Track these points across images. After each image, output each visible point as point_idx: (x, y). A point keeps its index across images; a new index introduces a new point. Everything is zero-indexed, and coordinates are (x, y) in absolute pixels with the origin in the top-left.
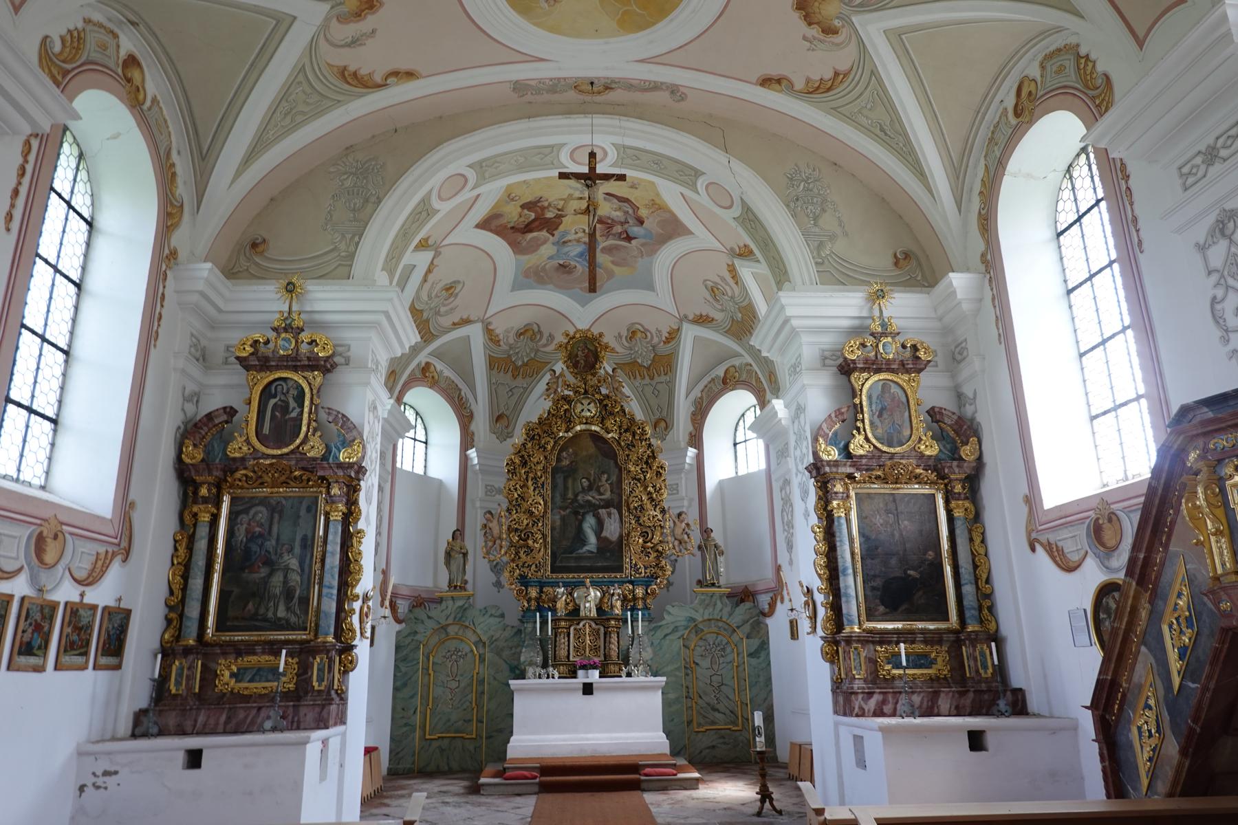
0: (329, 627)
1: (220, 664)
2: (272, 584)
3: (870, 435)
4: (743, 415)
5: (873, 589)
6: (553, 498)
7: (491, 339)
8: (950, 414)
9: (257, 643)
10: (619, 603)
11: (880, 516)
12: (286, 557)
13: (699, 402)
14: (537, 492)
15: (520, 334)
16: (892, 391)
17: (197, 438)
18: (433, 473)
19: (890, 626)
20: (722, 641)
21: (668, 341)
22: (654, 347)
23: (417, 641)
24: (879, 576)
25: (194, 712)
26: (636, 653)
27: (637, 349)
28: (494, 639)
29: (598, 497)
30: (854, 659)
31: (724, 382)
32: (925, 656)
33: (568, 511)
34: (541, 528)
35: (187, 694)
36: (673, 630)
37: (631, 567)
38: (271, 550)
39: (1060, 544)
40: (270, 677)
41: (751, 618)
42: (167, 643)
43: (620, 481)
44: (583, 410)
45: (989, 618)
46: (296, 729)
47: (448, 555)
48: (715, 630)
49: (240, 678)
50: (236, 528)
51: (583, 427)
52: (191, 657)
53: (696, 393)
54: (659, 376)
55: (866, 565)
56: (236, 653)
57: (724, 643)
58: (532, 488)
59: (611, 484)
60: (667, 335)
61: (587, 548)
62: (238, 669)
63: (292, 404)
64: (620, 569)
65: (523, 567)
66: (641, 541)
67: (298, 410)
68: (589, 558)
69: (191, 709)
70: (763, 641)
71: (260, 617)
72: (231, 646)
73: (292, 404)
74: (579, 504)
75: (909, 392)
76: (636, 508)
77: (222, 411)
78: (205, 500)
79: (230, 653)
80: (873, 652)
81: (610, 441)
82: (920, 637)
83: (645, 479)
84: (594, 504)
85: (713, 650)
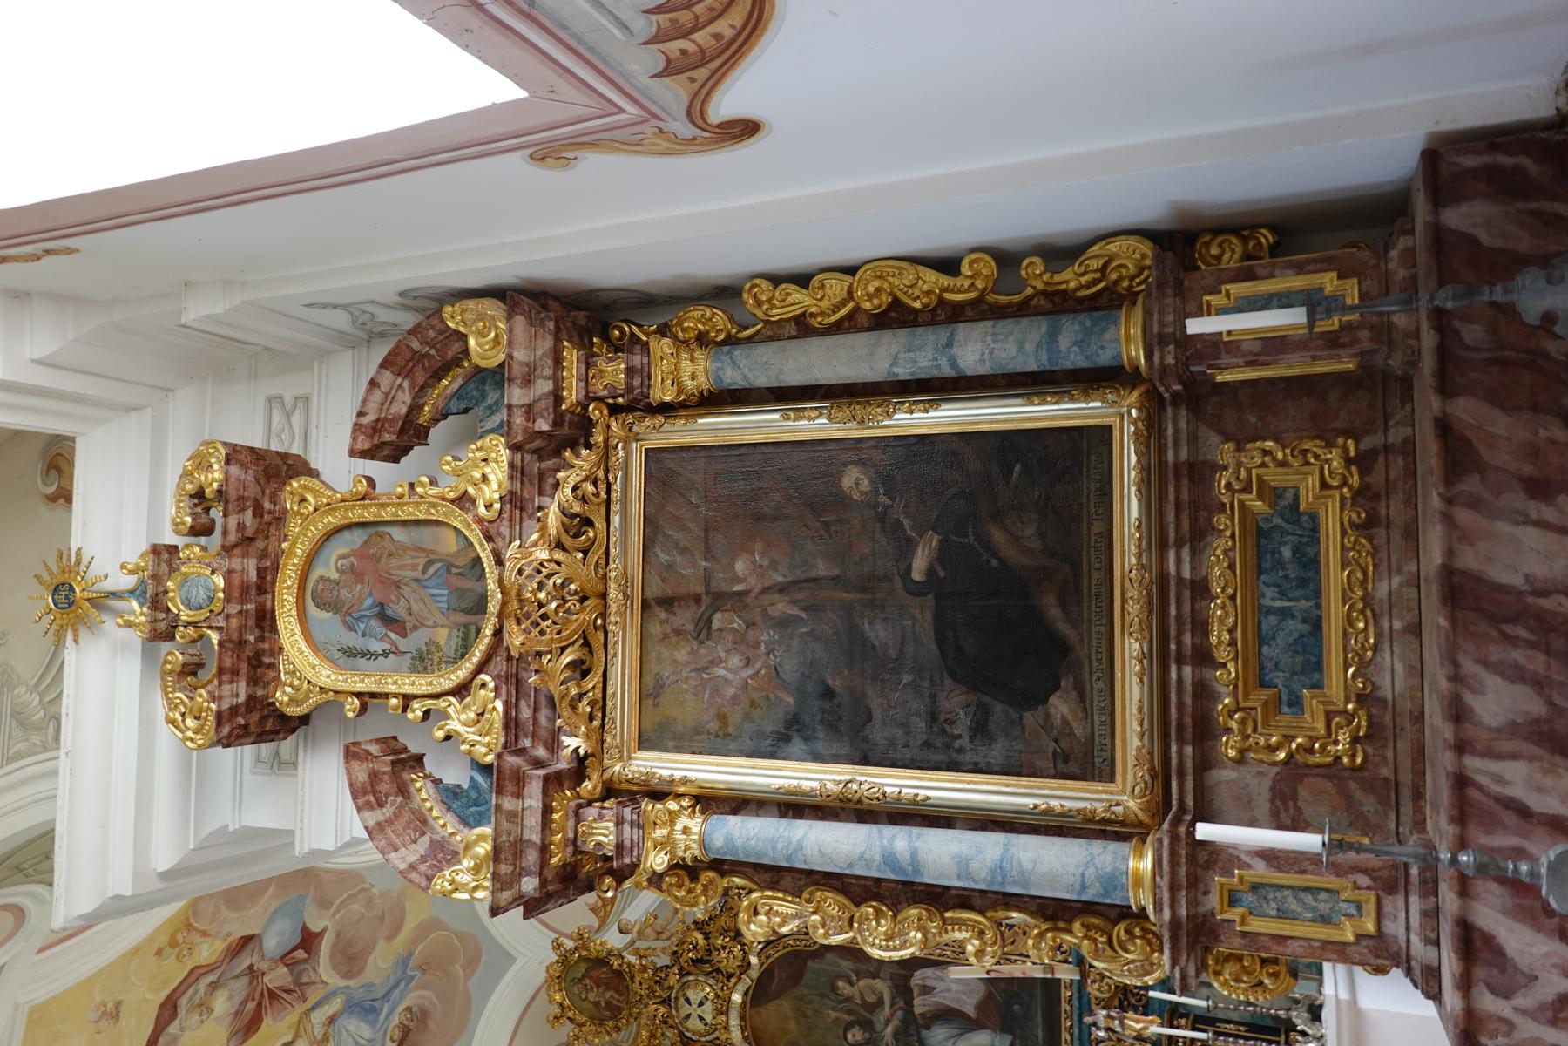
3: (447, 683)
5: (980, 729)
8: (378, 395)
11: (712, 663)
16: (335, 575)
19: (1132, 692)
24: (933, 698)
29: (887, 1011)
30: (1283, 915)
32: (1258, 537)
39: (644, 27)
45: (1095, 264)
46: (1318, 571)
51: (734, 1022)
55: (892, 743)
75: (332, 520)
80: (1246, 775)
82: (1179, 564)
84: (903, 1021)
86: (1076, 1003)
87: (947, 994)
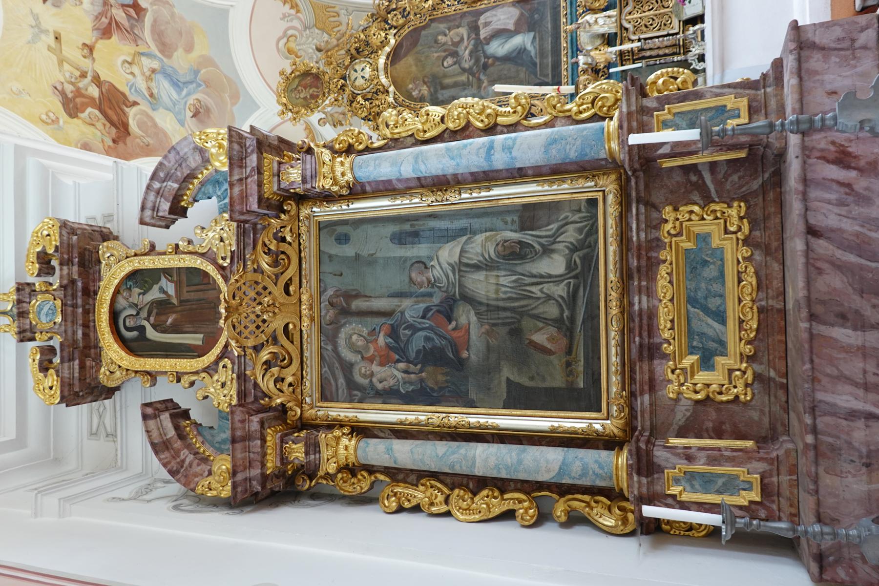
0: (589, 128)
1: (679, 393)
2: (493, 295)
9: (625, 309)
12: (437, 272)
17: (197, 469)
22: (306, 28)
25: (823, 422)
33: (482, 77)
35: (761, 459)
38: (423, 306)
40: (710, 272)
42: (625, 521)
43: (446, 19)
44: (363, 77)
49: (712, 345)
50: (380, 386)
52: (659, 454)
56: (651, 358)
59: (449, 29)
60: (288, 6)
61: (529, 47)
62: (692, 351)
63: (154, 294)
67: (164, 282)
68: (541, 39)
69: (814, 431)
71: (566, 313)
72: (632, 371)
73: (154, 294)
74: (474, 64)
77: (152, 423)
78: (313, 447)
79: (651, 372)
84: (474, 45)
86: (569, 16)
87: (498, 23)
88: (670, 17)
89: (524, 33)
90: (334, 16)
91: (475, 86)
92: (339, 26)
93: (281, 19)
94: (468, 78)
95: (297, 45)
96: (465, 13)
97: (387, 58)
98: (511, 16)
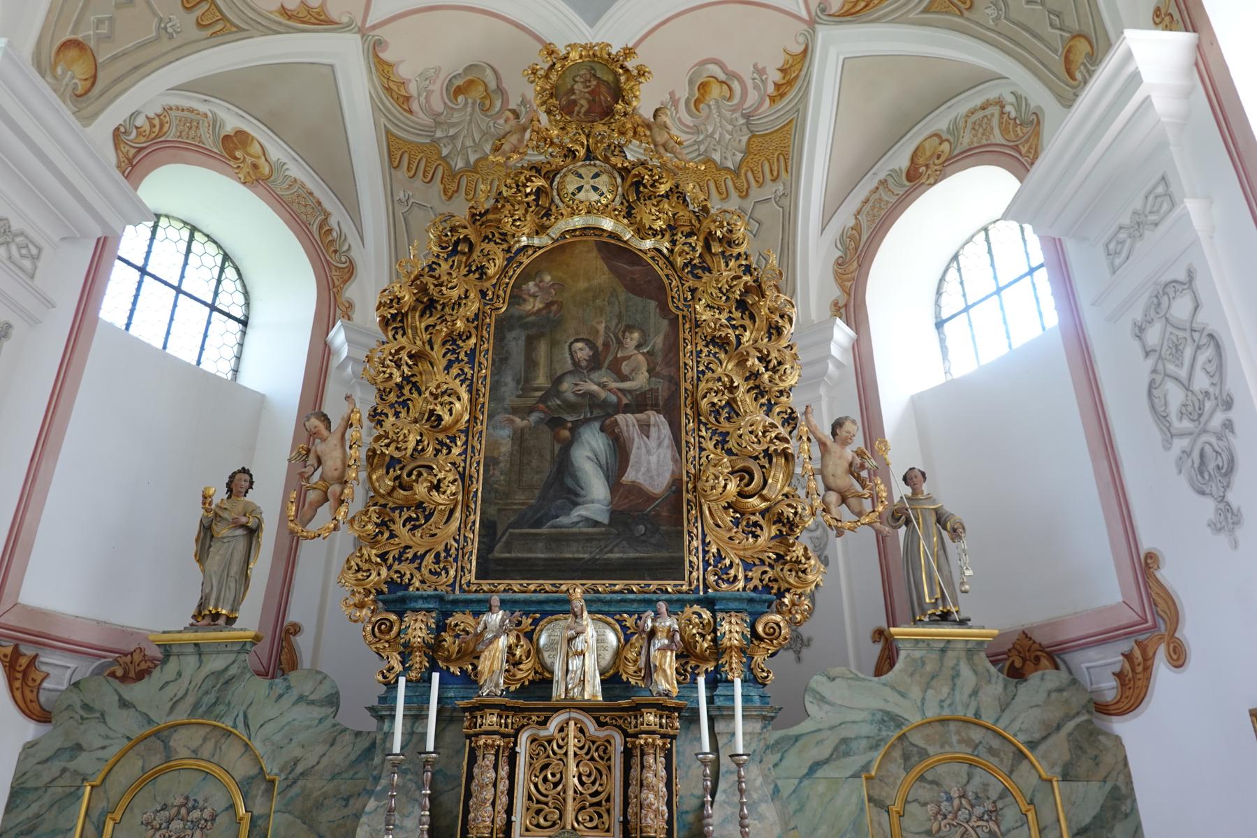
4: (955, 257)
6: (495, 387)
7: (389, 89)
10: (669, 662)
13: (851, 238)
14: (455, 371)
15: (457, 90)
18: (251, 379)
20: (986, 786)
21: (781, 90)
22: (747, 117)
23: (76, 773)
26: (725, 821)
27: (710, 129)
28: (299, 769)
29: (614, 385)
31: (910, 177)
33: (534, 417)
34: (459, 460)
36: (836, 749)
37: (706, 563)
41: (1069, 717)
43: (673, 347)
44: (580, 189)
47: (207, 534)
48: (963, 751)
53: (844, 218)
54: (761, 185)
57: (994, 795)
58: (444, 362)
59: (650, 354)
60: (778, 77)
64: (674, 568)
65: (399, 559)
66: (732, 487)
68: (589, 538)
70: (1115, 788)
74: (565, 401)
76: (715, 410)
81: (647, 258)
83: (739, 343)
85: (963, 814)
87: (644, 450)
88: (554, 824)
89: (611, 503)
90: (771, 171)
91: (519, 402)
92: (757, 182)
93: (755, 66)
94: (537, 389)
95: (717, 102)
96: (678, 385)
97: (612, 235)
98: (651, 477)
